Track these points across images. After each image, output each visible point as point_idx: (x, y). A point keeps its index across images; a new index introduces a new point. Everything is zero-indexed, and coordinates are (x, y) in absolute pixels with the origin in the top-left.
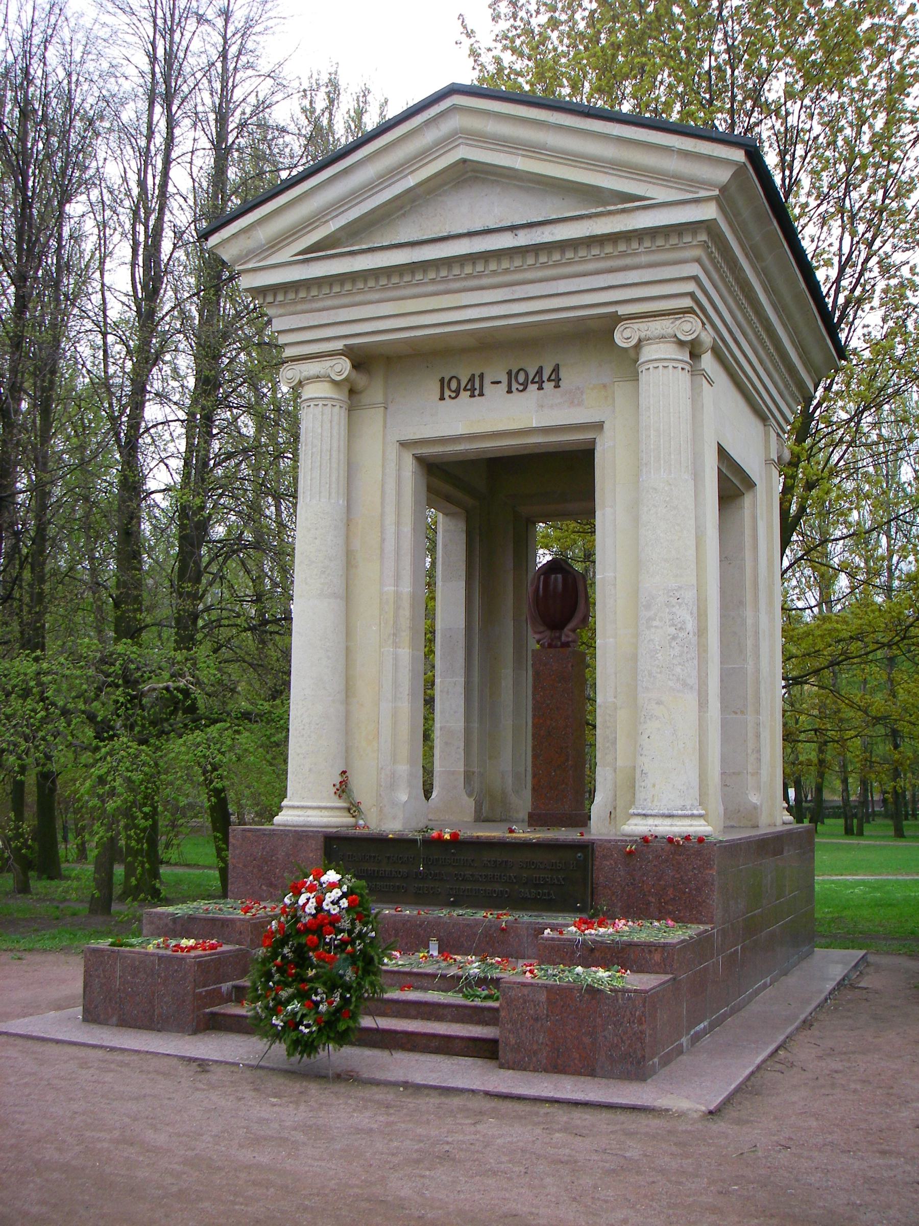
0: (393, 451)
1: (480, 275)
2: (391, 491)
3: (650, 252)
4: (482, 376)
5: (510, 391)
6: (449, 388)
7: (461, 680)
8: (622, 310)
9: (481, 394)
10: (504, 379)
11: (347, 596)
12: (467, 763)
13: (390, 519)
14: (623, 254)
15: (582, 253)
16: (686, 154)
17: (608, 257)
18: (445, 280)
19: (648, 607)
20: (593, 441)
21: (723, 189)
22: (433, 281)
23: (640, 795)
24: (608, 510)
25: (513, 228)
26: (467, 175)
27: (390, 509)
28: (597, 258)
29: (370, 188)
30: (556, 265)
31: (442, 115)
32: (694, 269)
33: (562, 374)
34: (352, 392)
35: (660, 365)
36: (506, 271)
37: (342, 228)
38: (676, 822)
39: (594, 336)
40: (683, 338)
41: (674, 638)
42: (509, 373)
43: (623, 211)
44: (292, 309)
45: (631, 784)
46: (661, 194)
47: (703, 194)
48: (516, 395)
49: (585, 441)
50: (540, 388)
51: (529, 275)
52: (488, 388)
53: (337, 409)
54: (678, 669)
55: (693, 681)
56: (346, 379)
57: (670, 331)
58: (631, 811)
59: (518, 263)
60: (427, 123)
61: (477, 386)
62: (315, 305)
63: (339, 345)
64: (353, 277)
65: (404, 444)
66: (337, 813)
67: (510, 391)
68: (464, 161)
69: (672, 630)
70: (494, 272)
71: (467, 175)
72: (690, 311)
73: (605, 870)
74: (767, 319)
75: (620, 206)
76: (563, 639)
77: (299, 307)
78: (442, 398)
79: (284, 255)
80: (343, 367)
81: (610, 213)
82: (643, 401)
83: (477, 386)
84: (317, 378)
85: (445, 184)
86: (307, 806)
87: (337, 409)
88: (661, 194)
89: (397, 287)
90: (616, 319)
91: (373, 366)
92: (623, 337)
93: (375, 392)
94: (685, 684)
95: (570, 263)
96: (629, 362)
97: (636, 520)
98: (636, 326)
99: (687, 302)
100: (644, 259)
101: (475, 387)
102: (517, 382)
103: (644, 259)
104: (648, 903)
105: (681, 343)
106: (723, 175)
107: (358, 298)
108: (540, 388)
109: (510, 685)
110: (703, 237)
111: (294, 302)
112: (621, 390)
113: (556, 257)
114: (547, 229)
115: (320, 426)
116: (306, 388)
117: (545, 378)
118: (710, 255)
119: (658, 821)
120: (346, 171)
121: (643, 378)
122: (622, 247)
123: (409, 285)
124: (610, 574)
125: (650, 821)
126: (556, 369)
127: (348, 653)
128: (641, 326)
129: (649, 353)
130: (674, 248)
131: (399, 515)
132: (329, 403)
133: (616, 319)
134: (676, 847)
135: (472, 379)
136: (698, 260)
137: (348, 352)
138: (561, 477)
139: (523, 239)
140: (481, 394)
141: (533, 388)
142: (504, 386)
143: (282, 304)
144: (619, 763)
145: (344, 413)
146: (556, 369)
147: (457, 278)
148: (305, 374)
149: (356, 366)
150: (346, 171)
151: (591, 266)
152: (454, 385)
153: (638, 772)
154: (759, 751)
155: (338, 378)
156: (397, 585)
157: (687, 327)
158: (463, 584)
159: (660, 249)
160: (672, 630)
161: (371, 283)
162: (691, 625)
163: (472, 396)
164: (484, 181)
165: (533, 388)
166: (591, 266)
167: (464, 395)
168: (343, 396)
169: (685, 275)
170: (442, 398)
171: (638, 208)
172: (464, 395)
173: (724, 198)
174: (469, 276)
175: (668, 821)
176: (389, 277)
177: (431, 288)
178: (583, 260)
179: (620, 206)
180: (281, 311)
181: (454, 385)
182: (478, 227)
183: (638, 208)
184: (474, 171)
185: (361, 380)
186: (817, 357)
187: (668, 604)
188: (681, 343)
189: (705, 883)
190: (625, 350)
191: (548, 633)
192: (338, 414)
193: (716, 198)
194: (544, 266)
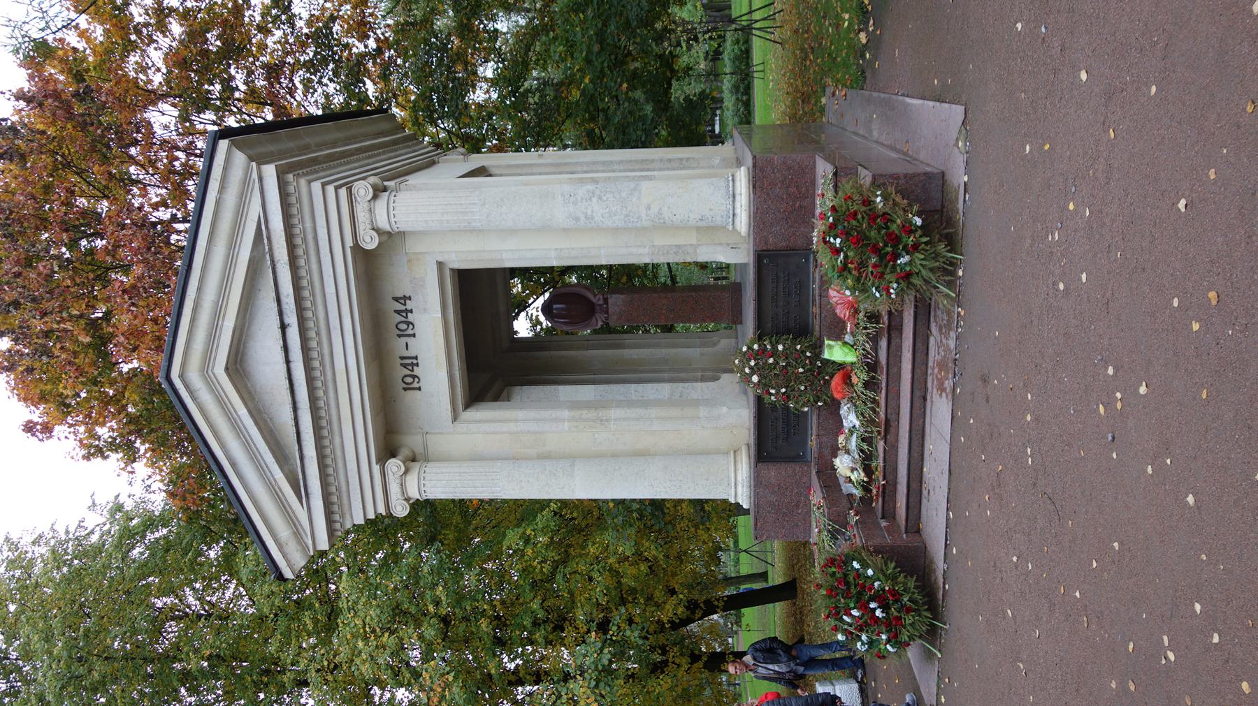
0: (459, 426)
1: (321, 355)
2: (495, 425)
3: (302, 220)
4: (402, 358)
5: (414, 335)
6: (412, 383)
7: (633, 386)
8: (349, 242)
9: (416, 358)
10: (404, 340)
11: (572, 457)
12: (696, 381)
13: (512, 427)
14: (305, 240)
15: (303, 273)
16: (222, 188)
17: (306, 252)
18: (325, 383)
19: (577, 219)
20: (452, 270)
21: (251, 159)
22: (325, 393)
23: (719, 221)
24: (504, 256)
25: (283, 327)
26: (238, 366)
27: (505, 427)
28: (308, 261)
29: (248, 445)
30: (313, 294)
31: (187, 386)
32: (316, 186)
33: (400, 294)
34: (414, 460)
35: (392, 213)
36: (318, 334)
37: (281, 468)
38: (738, 192)
39: (370, 265)
40: (371, 195)
41: (600, 198)
42: (399, 336)
43: (269, 238)
44: (346, 508)
45: (708, 230)
46: (255, 209)
47: (255, 175)
48: (416, 331)
49: (453, 277)
50: (411, 311)
51: (326, 351)
52: (411, 353)
53: (427, 470)
54: (623, 194)
55: (632, 185)
56: (404, 463)
57: (366, 205)
58: (730, 228)
59: (311, 324)
60: (194, 399)
61: (409, 361)
62: (344, 488)
63: (376, 469)
64: (321, 457)
65: (455, 418)
66: (738, 458)
67: (414, 335)
68: (227, 369)
69: (595, 200)
70: (319, 343)
71: (238, 366)
72: (350, 190)
73: (775, 241)
74: (356, 149)
75: (266, 241)
76: (601, 302)
77: (345, 501)
78: (419, 389)
79: (302, 514)
80: (394, 465)
81: (271, 249)
82: (419, 227)
83: (409, 361)
84: (403, 486)
85: (246, 385)
86: (733, 481)
87: (427, 470)
88: (255, 209)
89: (330, 422)
90: (357, 248)
91: (390, 442)
92: (370, 242)
93: (412, 441)
94: (635, 189)
95: (311, 282)
96: (390, 238)
97: (512, 232)
98: (362, 232)
99: (343, 192)
100: (308, 225)
101: (411, 363)
102: (406, 330)
103: (308, 225)
104: (801, 207)
105: (375, 197)
106: (240, 158)
107: (339, 453)
108: (411, 311)
109: (636, 351)
110: (290, 177)
111: (341, 506)
112: (413, 246)
113: (306, 293)
114: (284, 299)
115: (440, 484)
116: (411, 495)
117: (403, 308)
118: (308, 174)
119: (738, 205)
120: (234, 465)
121: (403, 227)
122: (298, 241)
123: (328, 412)
124: (553, 254)
125: (738, 211)
126: (396, 299)
127: (615, 455)
128: (362, 228)
129: (383, 223)
130: (299, 200)
131: (510, 421)
132: (422, 475)
133: (357, 248)
134: (758, 183)
135: (404, 366)
136: (309, 182)
137: (382, 460)
138: (480, 296)
139: (291, 319)
140: (416, 358)
141: (411, 317)
142: (410, 340)
143: (342, 516)
144: (694, 242)
145: (430, 465)
146: (396, 299)
147: (323, 373)
148: (399, 496)
149: (394, 455)
150: (234, 465)
151: (314, 266)
152: (409, 380)
153: (701, 224)
154: (681, 159)
155: (403, 469)
156: (563, 420)
157: (362, 192)
158: (561, 387)
159: (300, 211)
160: (595, 200)
161: (326, 442)
162: (590, 187)
163: (417, 365)
164: (243, 355)
165: (411, 317)
166: (314, 266)
167: (417, 371)
168: (416, 466)
169: (321, 192)
170: (419, 389)
171: (267, 228)
172: (417, 371)
173: (261, 160)
174: (322, 363)
175: (738, 197)
176: (321, 428)
177: (331, 394)
178: (310, 272)
179: (266, 241)
180: (348, 517)
181: (409, 380)
182: (280, 356)
183: (267, 228)
184: (236, 363)
185: (405, 452)
186: (385, 126)
187: (575, 203)
188: (375, 197)
189: (784, 163)
190: (380, 244)
191: (597, 315)
192: (431, 468)
193: (259, 164)
194: (314, 303)
